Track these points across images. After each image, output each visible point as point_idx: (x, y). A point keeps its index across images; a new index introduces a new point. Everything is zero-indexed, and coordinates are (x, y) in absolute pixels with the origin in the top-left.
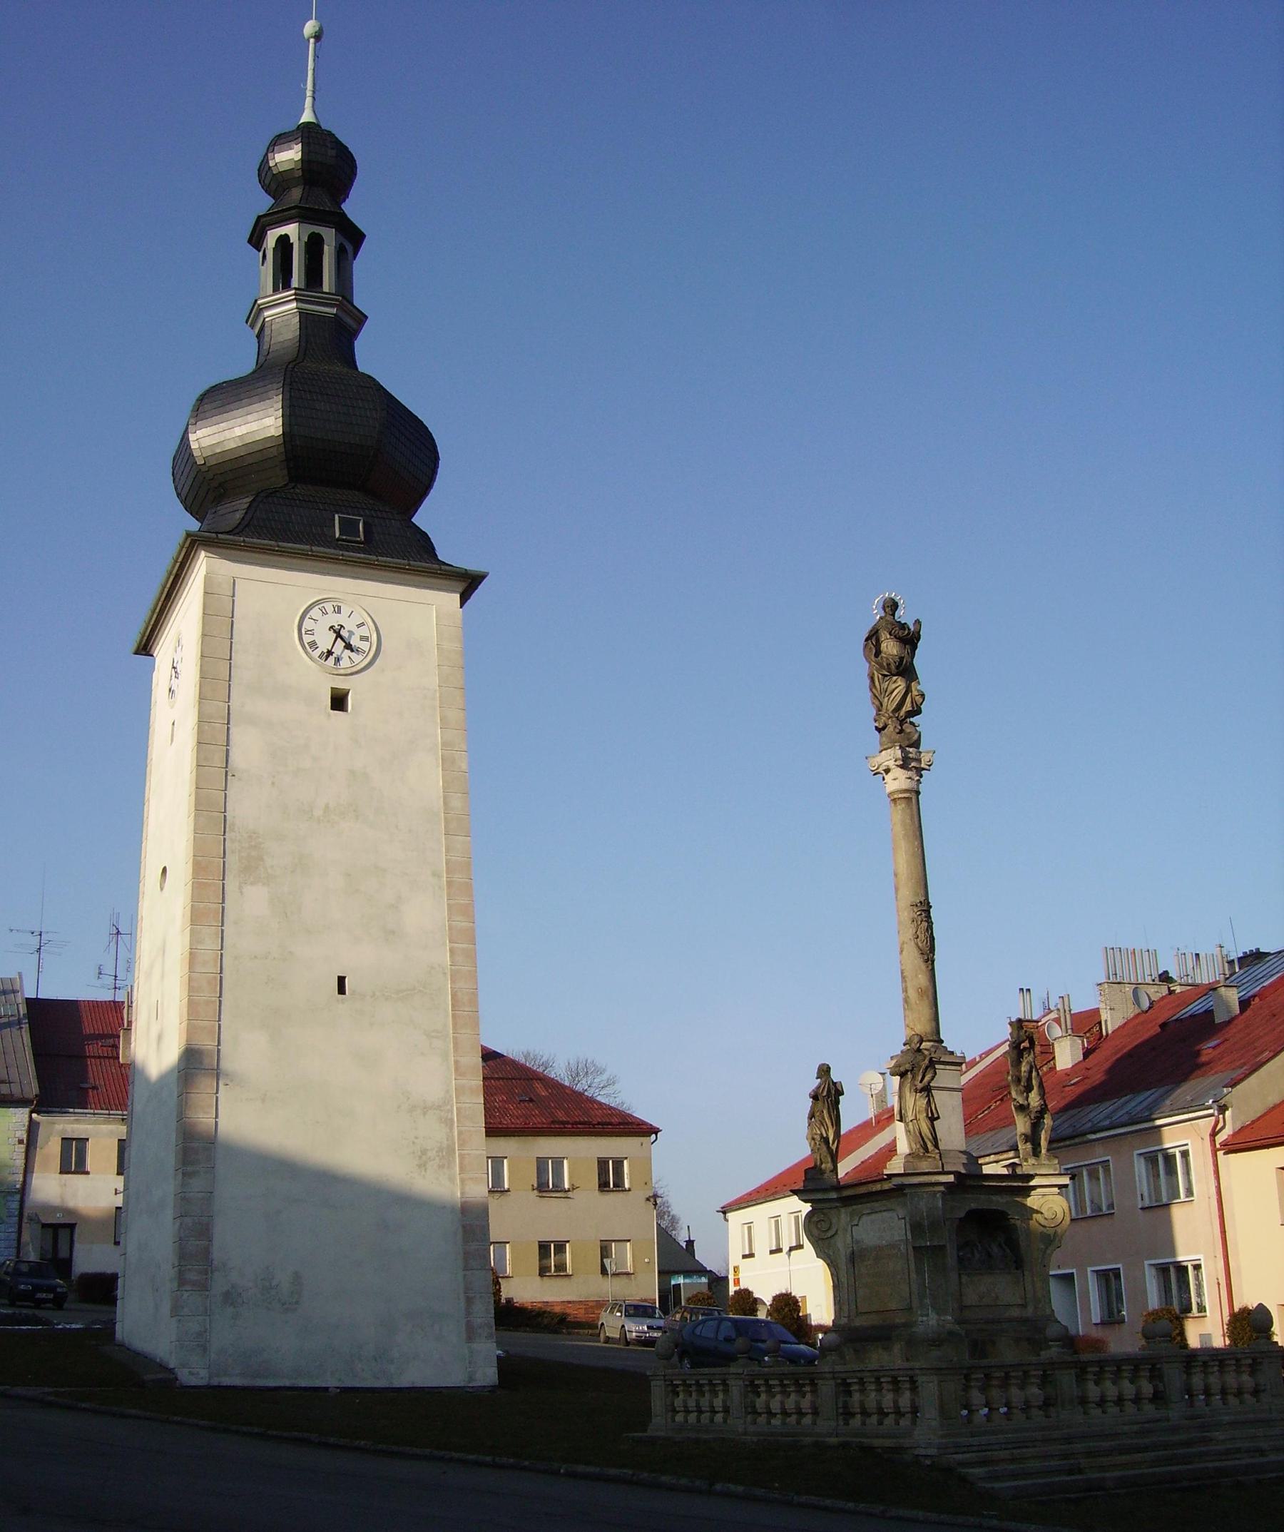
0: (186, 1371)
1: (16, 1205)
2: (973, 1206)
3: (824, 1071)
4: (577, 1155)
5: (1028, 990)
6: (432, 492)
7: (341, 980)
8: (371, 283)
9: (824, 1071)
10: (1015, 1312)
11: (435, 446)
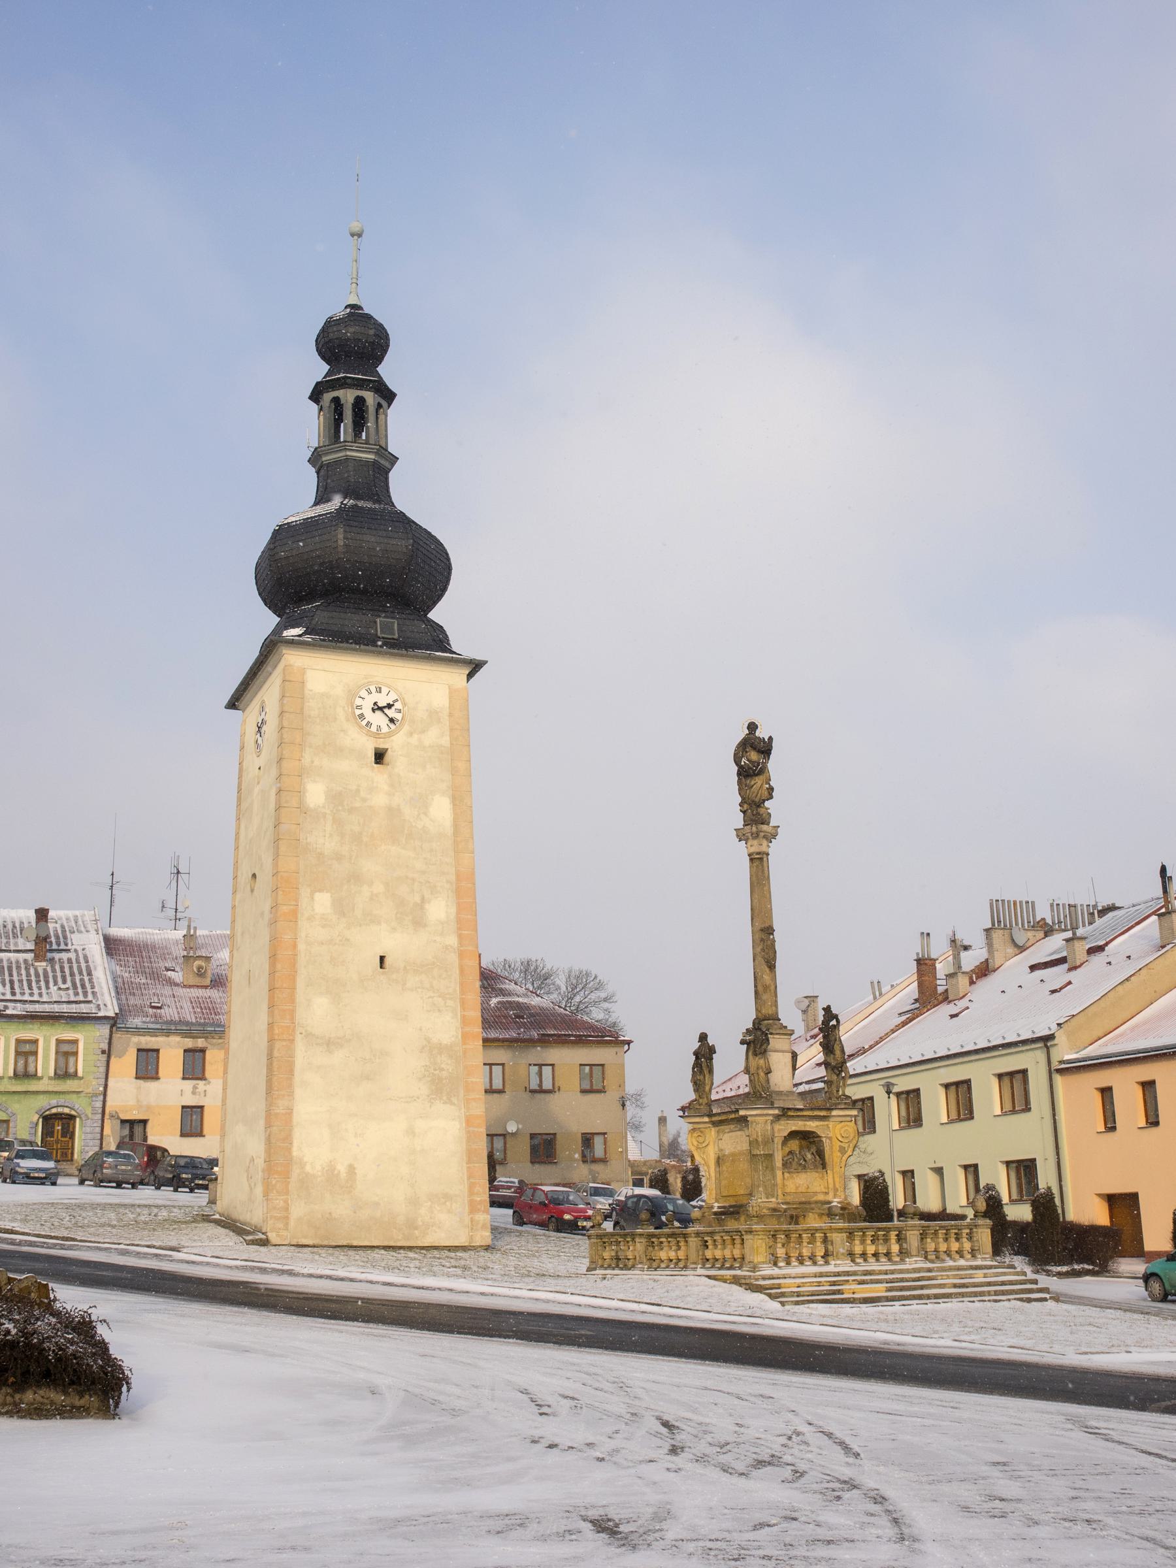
0: (274, 1234)
1: (99, 1104)
2: (794, 1128)
3: (703, 1037)
4: (568, 1059)
5: (928, 934)
6: (450, 587)
7: (382, 958)
8: (401, 427)
9: (703, 1037)
10: (821, 1197)
11: (448, 559)
